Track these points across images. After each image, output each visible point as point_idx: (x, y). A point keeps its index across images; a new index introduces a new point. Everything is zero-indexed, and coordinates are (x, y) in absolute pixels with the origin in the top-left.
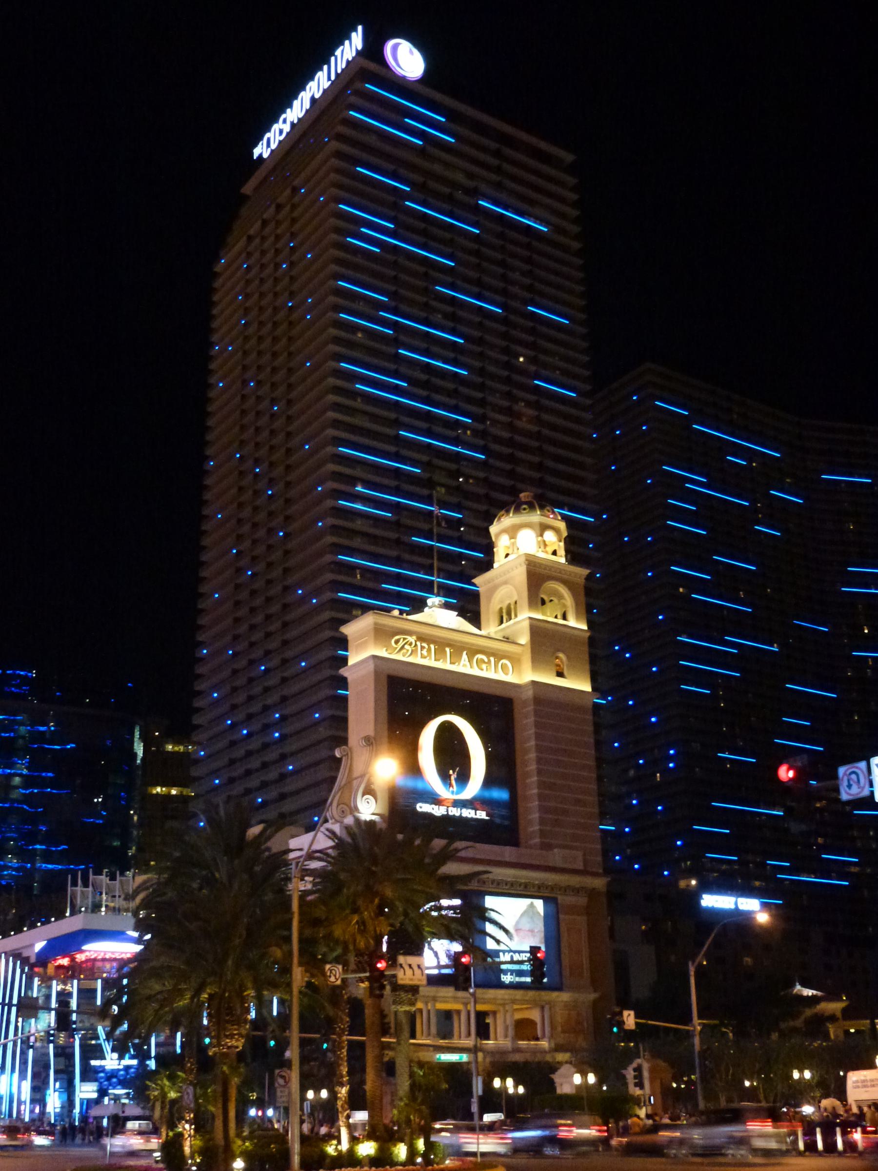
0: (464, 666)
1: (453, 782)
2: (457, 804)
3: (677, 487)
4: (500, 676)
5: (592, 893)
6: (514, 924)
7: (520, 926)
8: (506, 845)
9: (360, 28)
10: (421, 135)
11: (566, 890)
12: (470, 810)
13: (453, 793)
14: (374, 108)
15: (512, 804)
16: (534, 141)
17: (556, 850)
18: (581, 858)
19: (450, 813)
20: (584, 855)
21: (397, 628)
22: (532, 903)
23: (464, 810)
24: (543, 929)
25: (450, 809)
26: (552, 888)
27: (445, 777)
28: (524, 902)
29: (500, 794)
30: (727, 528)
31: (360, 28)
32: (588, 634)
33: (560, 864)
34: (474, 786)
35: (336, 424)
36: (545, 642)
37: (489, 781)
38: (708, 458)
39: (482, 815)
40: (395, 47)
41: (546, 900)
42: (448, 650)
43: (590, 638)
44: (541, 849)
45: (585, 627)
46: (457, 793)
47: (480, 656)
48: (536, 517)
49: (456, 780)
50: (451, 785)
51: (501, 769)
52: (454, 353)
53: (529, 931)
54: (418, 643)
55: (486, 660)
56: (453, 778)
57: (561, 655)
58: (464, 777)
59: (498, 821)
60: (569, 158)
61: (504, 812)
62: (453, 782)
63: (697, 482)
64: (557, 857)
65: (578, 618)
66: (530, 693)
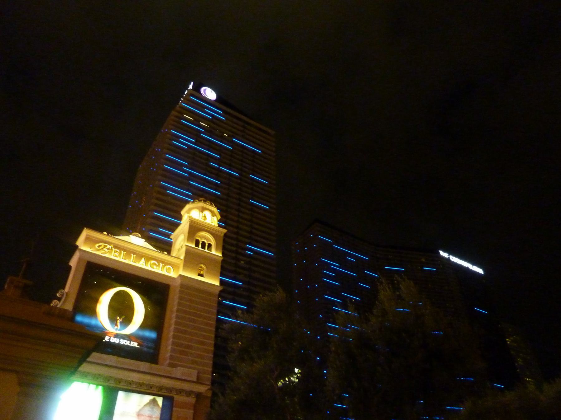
0: (141, 264)
1: (118, 324)
2: (117, 336)
3: (327, 267)
4: (164, 272)
5: (199, 396)
6: (138, 410)
7: (142, 413)
8: (141, 360)
9: (192, 83)
10: (212, 115)
11: (180, 392)
12: (125, 341)
13: (116, 329)
14: (196, 106)
15: (157, 343)
16: (258, 125)
17: (179, 368)
18: (196, 375)
19: (111, 341)
20: (198, 373)
21: (99, 239)
22: (154, 399)
23: (122, 340)
24: (159, 416)
25: (112, 338)
26: (170, 390)
27: (113, 320)
28: (148, 398)
29: (152, 335)
30: (348, 285)
31: (192, 83)
32: (222, 259)
33: (179, 376)
34: (134, 327)
35: (156, 205)
36: (191, 258)
37: (143, 326)
38: (340, 258)
39: (135, 344)
40: (205, 90)
41: (165, 398)
42: (132, 255)
43: (223, 261)
44: (169, 366)
45: (221, 255)
46: (119, 330)
47: (153, 262)
48: (201, 204)
49: (120, 323)
50: (116, 325)
51: (155, 321)
52: (216, 187)
53: (148, 416)
54: (114, 249)
55: (157, 264)
56: (118, 321)
57: (203, 266)
58: (127, 321)
59: (145, 349)
60: (273, 133)
61: (150, 345)
62: (118, 324)
63: (335, 265)
64: (178, 372)
65: (217, 249)
66: (179, 282)
